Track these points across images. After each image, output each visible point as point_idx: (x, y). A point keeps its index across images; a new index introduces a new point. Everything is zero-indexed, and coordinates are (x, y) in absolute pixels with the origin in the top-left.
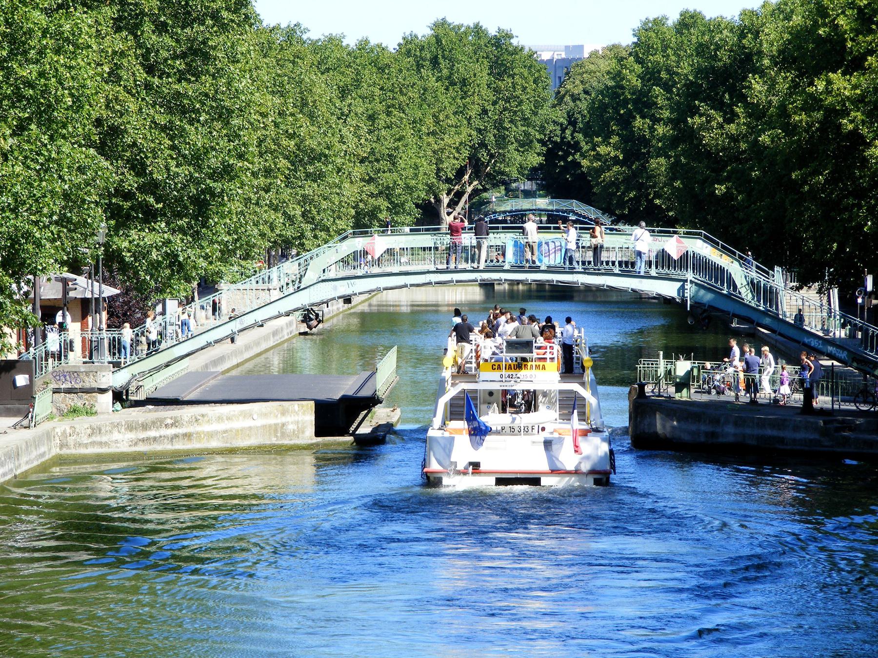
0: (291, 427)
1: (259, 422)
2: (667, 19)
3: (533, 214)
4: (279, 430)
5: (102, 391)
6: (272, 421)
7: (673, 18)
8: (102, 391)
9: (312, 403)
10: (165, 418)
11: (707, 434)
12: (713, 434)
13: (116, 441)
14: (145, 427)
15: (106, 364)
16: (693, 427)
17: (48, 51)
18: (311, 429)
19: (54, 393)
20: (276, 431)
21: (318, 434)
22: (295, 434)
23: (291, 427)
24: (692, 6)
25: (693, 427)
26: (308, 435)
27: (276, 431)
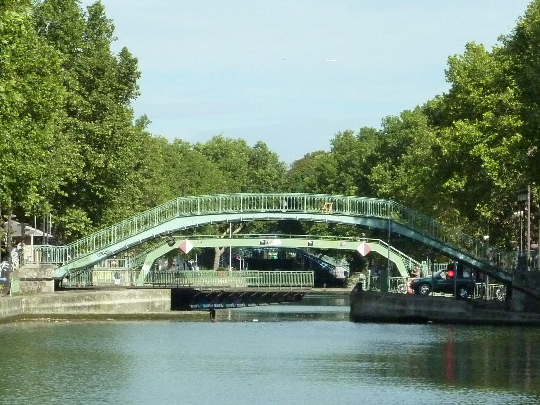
0: (157, 304)
1: (140, 300)
2: (353, 133)
3: (457, 111)
4: (150, 305)
5: (49, 280)
6: (146, 300)
7: (356, 133)
8: (49, 280)
9: (169, 291)
10: (85, 295)
11: (399, 311)
12: (402, 311)
13: (57, 308)
14: (73, 300)
15: (51, 264)
16: (390, 307)
17: (113, 123)
18: (168, 306)
19: (20, 280)
20: (148, 306)
21: (173, 308)
22: (159, 308)
23: (157, 304)
24: (363, 126)
25: (390, 307)
26: (167, 309)
27: (148, 306)
